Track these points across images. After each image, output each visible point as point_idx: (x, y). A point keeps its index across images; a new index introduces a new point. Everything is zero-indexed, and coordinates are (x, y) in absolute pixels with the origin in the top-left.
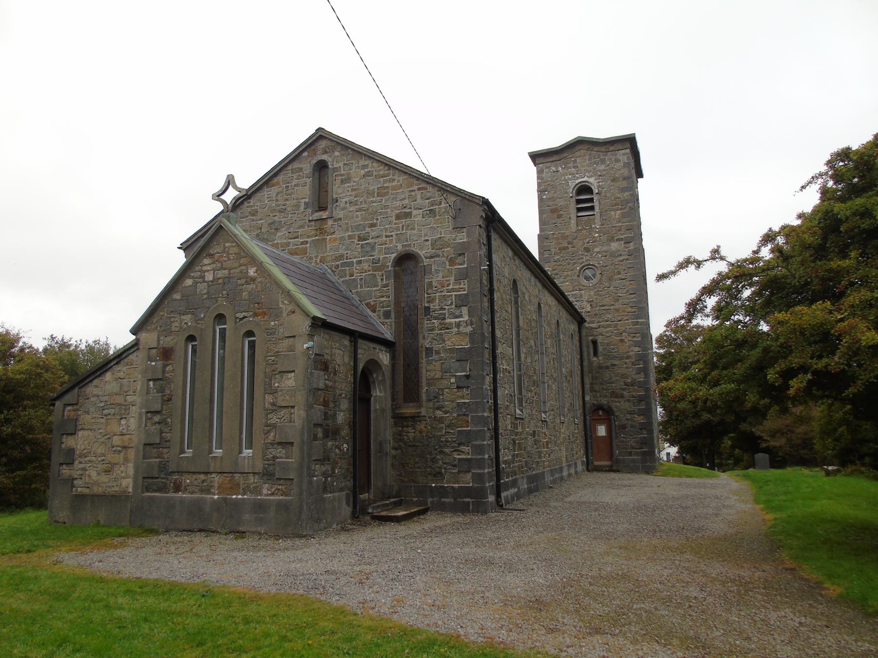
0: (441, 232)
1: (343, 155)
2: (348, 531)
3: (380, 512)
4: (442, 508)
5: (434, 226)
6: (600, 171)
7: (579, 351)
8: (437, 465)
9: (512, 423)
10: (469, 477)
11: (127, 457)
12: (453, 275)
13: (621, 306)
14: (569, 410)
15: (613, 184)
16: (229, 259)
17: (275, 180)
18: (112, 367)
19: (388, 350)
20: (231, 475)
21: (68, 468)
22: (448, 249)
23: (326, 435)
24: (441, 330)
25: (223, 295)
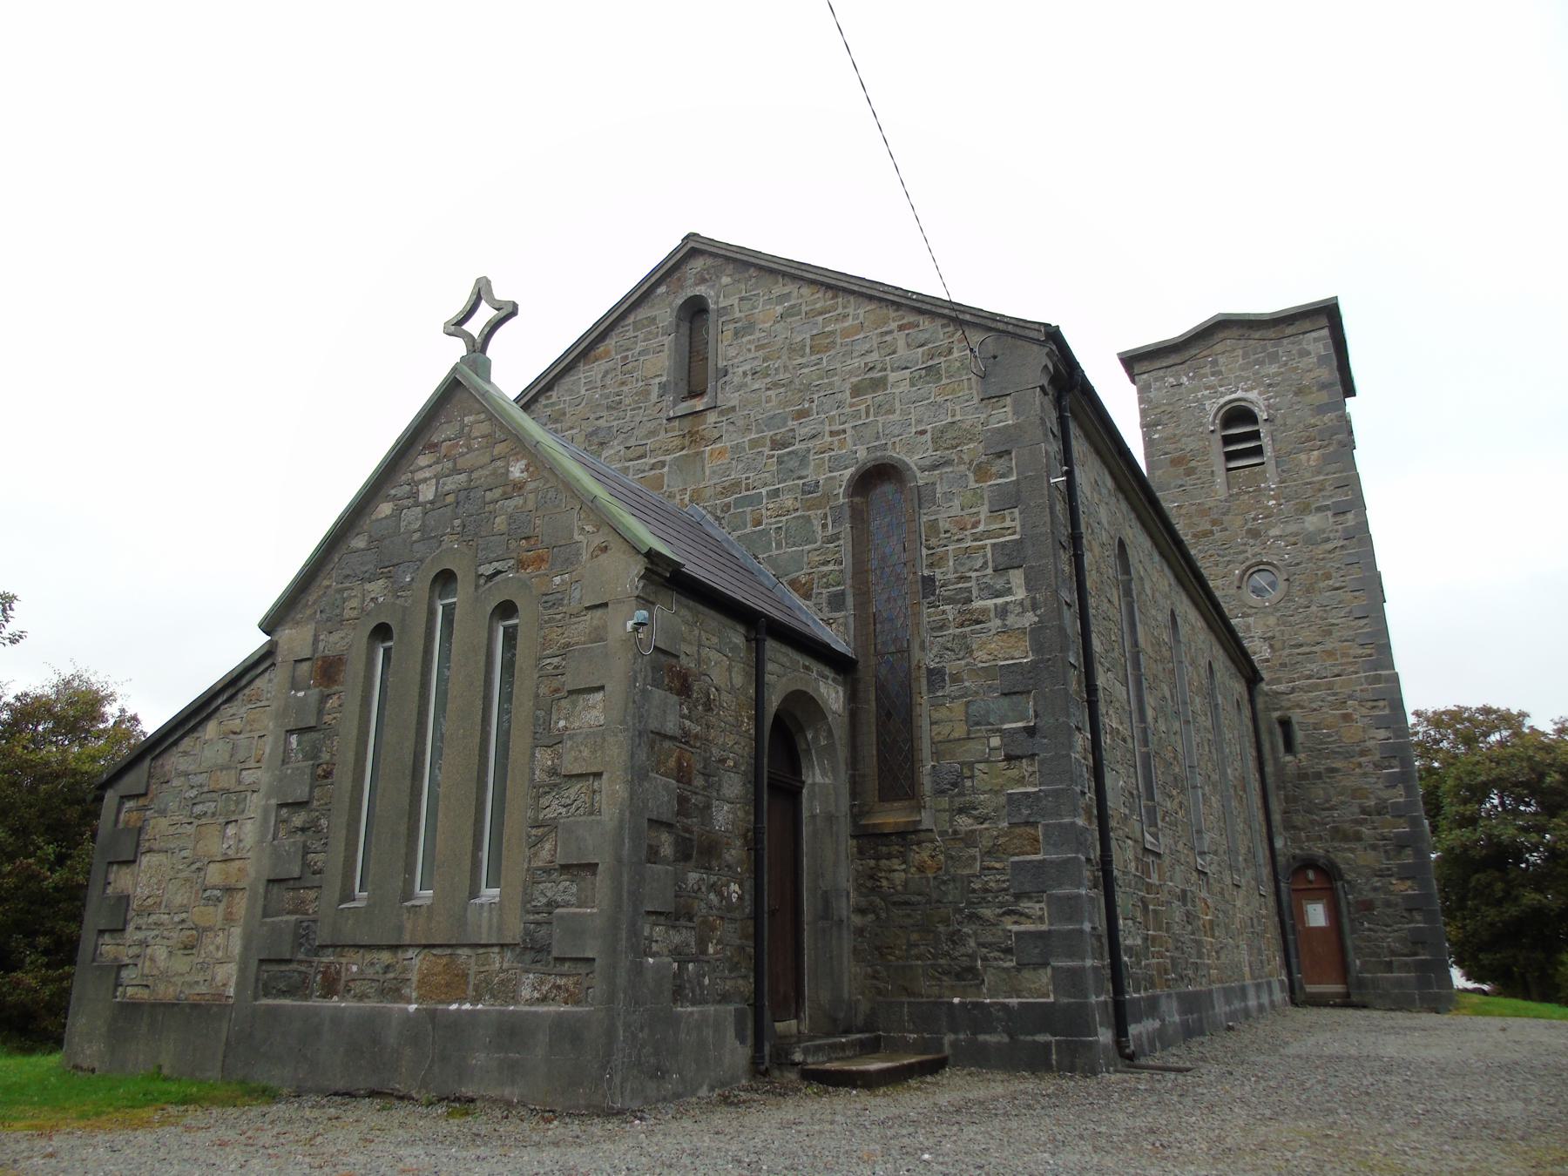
0: (954, 411)
1: (739, 281)
2: (737, 1105)
3: (824, 1063)
4: (978, 1059)
5: (938, 399)
6: (1268, 376)
7: (1253, 740)
8: (963, 950)
9: (1137, 859)
10: (1045, 980)
11: (231, 913)
12: (986, 502)
13: (1337, 645)
14: (1245, 860)
15: (1299, 399)
16: (470, 449)
17: (601, 348)
18: (217, 708)
19: (840, 678)
20: (449, 951)
21: (113, 942)
22: (972, 446)
23: (684, 853)
24: (962, 625)
25: (453, 528)
